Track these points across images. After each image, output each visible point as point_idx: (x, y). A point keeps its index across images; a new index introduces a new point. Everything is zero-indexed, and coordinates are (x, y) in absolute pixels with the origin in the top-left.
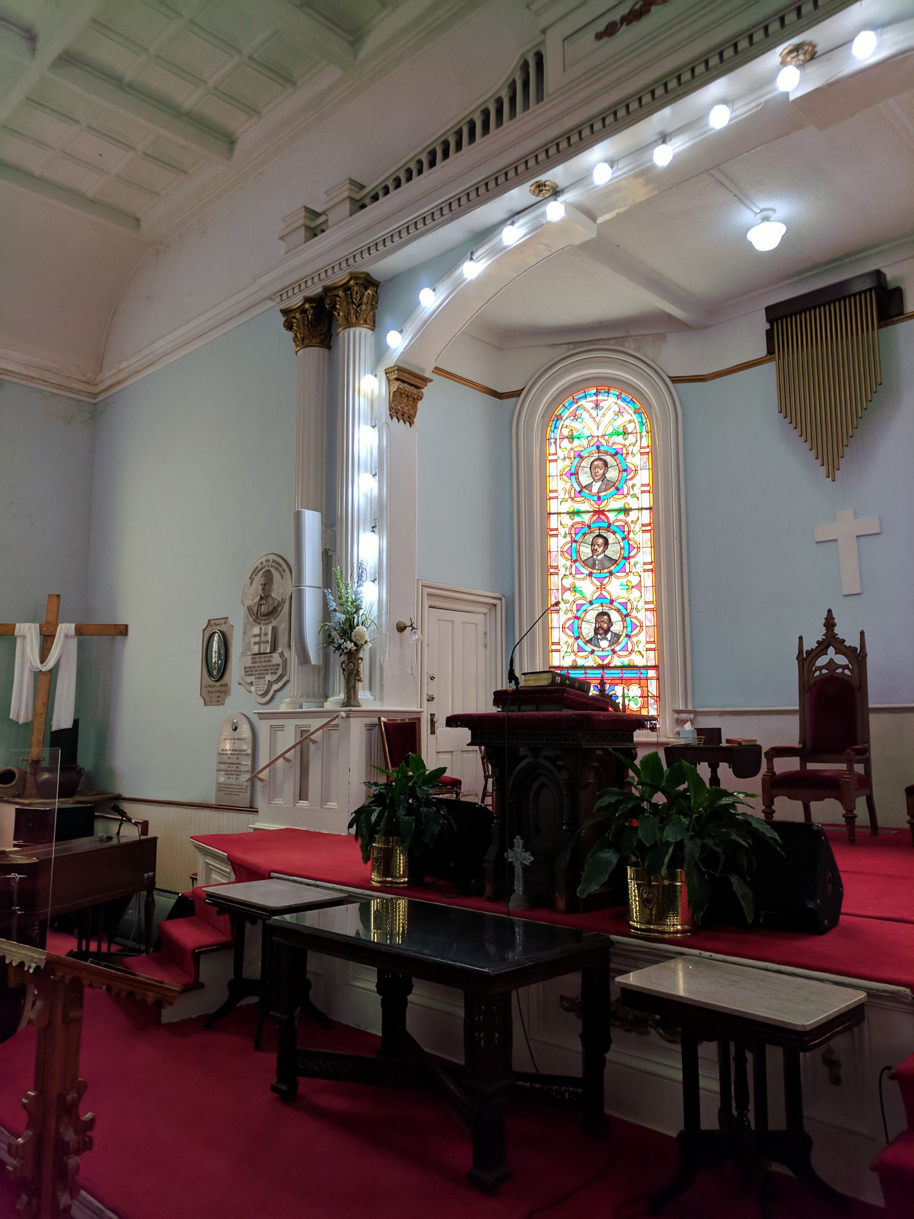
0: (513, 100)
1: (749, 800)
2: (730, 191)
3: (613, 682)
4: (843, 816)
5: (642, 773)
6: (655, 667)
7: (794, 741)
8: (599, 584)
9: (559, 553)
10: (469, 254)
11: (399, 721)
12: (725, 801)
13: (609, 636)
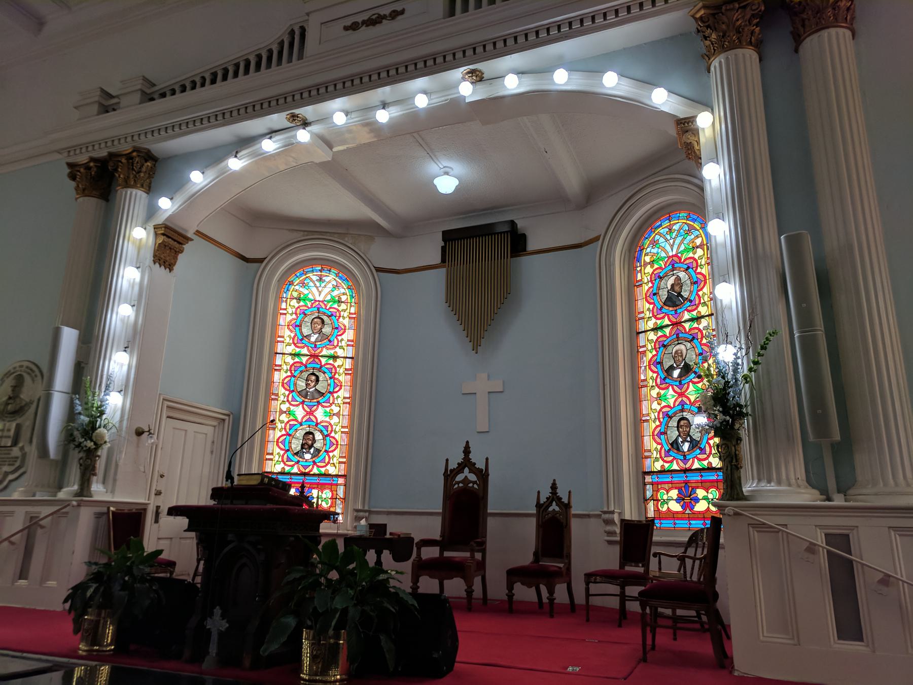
0: (280, 53)
1: (398, 576)
2: (425, 150)
3: (311, 486)
4: (466, 590)
5: (322, 554)
6: (344, 476)
7: (436, 535)
8: (309, 410)
9: (281, 384)
10: (234, 153)
11: (126, 511)
12: (382, 577)
13: (312, 450)
